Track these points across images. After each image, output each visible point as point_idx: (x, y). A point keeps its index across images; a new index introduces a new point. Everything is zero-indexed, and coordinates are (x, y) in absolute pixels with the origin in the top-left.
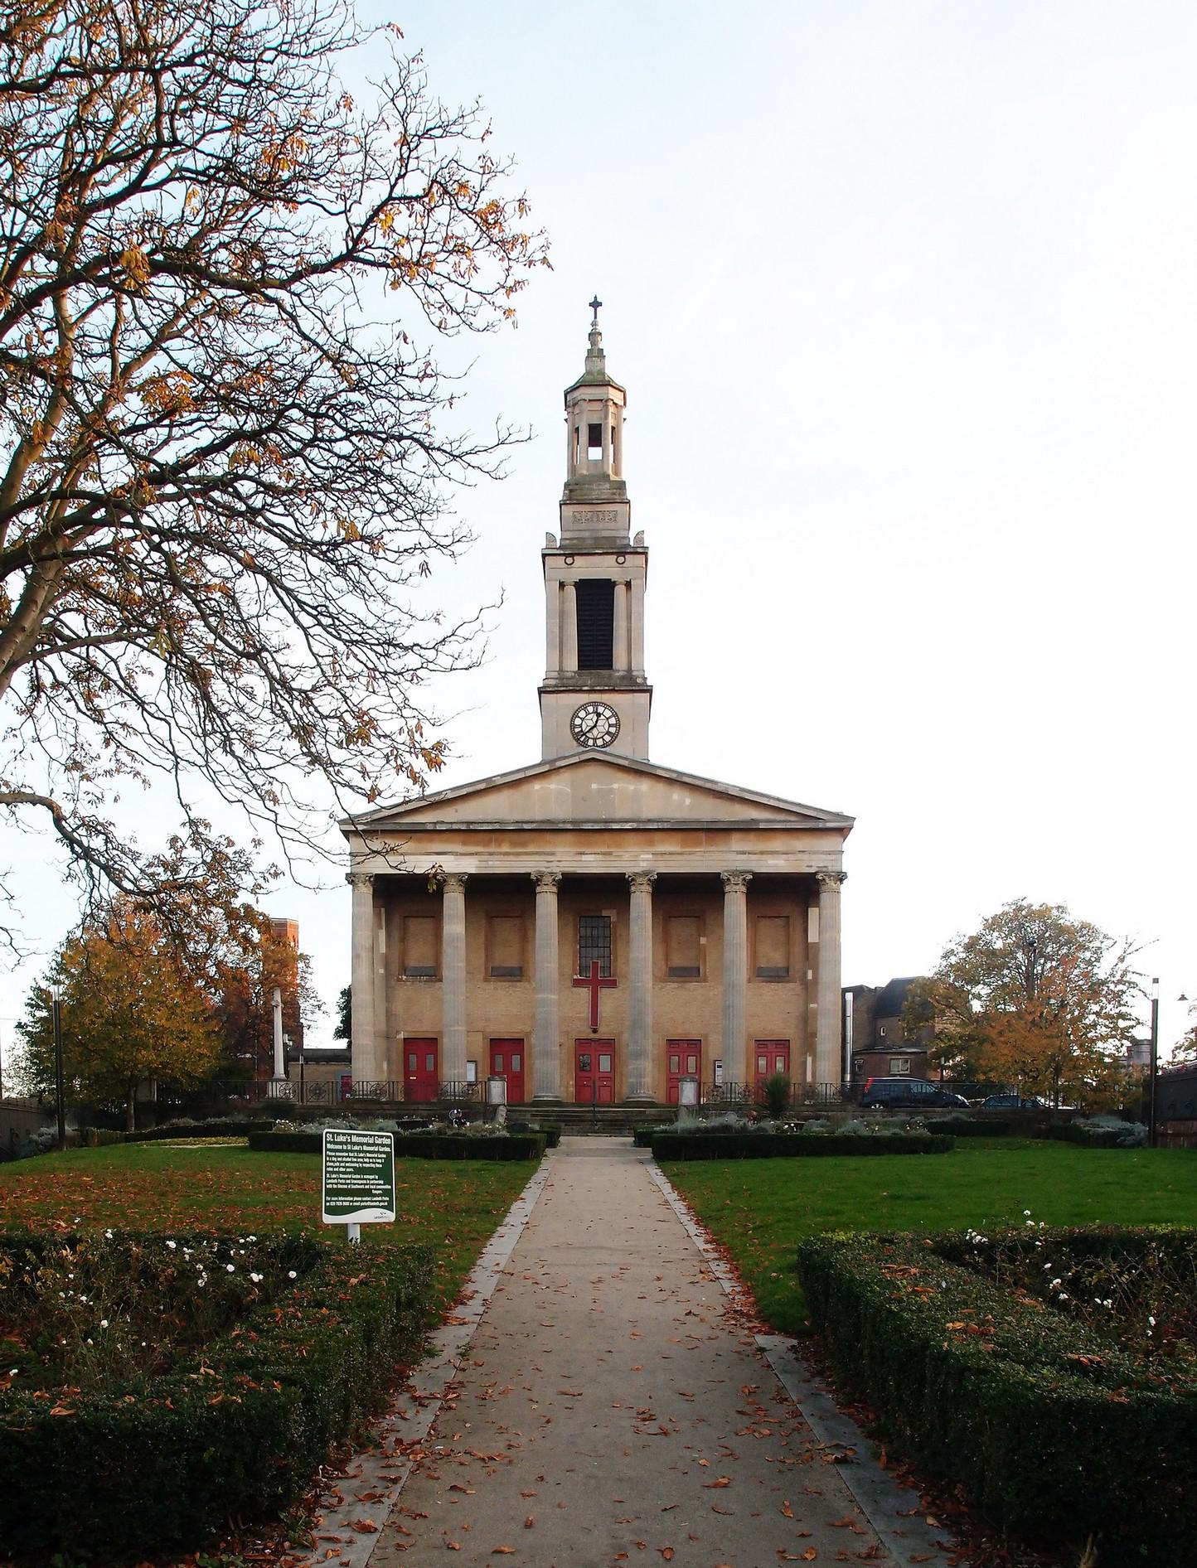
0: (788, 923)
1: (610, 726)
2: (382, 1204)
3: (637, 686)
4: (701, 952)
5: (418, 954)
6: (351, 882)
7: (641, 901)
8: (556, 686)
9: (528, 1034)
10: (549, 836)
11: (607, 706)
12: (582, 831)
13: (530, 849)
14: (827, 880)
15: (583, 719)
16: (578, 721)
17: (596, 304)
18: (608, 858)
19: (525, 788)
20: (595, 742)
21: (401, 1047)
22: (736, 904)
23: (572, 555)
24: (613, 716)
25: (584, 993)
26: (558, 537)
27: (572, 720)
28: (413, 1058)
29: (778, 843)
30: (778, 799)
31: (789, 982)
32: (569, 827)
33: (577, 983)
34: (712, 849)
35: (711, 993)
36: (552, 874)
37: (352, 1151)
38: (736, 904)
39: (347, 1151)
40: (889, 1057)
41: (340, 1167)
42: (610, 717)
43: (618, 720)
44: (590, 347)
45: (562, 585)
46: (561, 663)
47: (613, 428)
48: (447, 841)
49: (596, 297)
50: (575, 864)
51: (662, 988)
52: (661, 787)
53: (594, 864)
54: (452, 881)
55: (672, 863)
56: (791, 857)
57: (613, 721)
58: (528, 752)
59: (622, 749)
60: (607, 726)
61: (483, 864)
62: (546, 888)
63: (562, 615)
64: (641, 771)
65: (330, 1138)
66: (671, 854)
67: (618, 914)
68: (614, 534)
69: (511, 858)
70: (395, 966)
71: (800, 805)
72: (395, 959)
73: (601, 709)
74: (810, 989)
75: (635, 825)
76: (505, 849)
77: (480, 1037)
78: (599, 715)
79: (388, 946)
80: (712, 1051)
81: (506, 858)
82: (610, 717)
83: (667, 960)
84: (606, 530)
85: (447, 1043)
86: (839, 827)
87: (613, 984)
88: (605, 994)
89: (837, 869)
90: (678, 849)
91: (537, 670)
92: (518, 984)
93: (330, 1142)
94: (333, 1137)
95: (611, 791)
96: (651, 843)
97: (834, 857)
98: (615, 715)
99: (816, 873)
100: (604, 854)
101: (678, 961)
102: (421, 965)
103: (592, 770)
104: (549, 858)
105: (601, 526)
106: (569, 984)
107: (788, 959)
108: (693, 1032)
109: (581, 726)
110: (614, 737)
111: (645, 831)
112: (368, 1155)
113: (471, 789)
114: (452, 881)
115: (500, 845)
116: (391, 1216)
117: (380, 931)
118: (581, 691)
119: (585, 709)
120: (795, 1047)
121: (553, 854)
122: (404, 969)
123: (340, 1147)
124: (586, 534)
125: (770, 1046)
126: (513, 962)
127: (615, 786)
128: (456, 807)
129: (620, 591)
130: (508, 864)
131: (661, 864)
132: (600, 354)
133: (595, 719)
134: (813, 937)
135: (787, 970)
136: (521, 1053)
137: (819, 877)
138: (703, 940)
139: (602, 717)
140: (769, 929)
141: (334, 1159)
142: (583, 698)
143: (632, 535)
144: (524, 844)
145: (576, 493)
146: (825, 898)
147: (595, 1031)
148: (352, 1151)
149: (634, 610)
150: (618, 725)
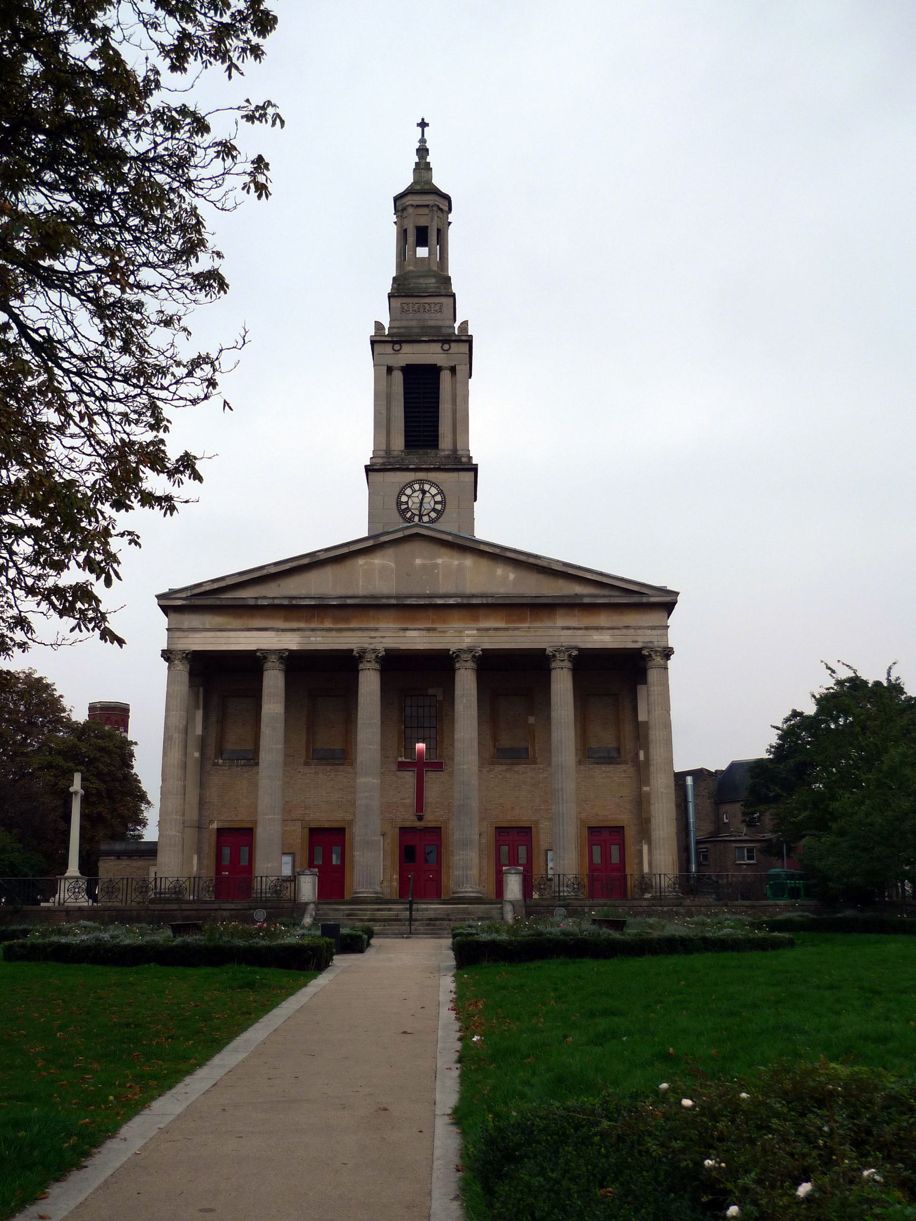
1: (436, 503)
5: (235, 738)
8: (383, 464)
11: (432, 484)
15: (409, 497)
17: (423, 125)
19: (349, 564)
23: (400, 342)
27: (399, 497)
28: (226, 851)
29: (603, 619)
36: (374, 651)
42: (436, 495)
43: (444, 497)
45: (390, 370)
52: (484, 564)
53: (418, 640)
54: (273, 658)
57: (438, 498)
59: (448, 526)
63: (389, 398)
68: (440, 323)
69: (334, 634)
70: (211, 751)
73: (427, 487)
78: (424, 492)
82: (436, 495)
85: (261, 835)
88: (430, 777)
89: (662, 644)
95: (436, 566)
96: (476, 619)
97: (659, 632)
98: (441, 492)
100: (428, 630)
103: (417, 547)
104: (373, 634)
105: (427, 316)
109: (407, 503)
110: (440, 513)
114: (273, 658)
118: (408, 470)
119: (411, 487)
124: (414, 323)
127: (439, 561)
129: (445, 376)
130: (330, 640)
131: (486, 639)
133: (421, 496)
139: (428, 495)
142: (410, 476)
144: (347, 620)
147: (420, 818)
150: (443, 502)
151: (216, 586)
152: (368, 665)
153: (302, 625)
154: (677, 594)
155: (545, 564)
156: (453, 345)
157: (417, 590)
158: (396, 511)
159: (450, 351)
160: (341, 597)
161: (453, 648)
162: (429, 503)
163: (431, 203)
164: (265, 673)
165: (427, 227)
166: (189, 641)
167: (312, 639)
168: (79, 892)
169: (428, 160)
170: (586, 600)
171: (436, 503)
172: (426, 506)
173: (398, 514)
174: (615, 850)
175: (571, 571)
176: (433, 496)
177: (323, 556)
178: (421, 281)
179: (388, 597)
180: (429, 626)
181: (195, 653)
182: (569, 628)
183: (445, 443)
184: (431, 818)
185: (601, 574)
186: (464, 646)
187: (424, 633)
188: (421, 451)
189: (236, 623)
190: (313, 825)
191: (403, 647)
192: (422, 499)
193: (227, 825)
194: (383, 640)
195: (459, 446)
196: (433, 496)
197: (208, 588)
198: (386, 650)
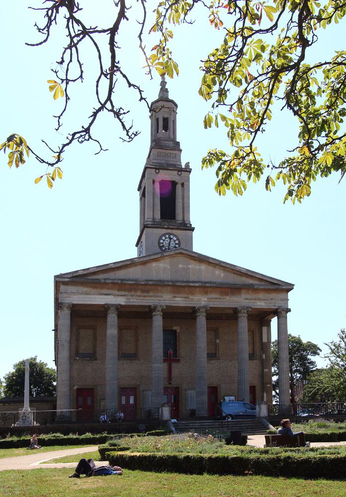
8: (152, 224)
9: (139, 386)
11: (175, 235)
12: (176, 287)
13: (151, 294)
15: (164, 240)
19: (148, 265)
23: (159, 169)
24: (177, 240)
27: (159, 240)
29: (261, 295)
31: (254, 360)
32: (170, 284)
34: (156, 294)
35: (221, 365)
43: (179, 242)
45: (154, 182)
46: (153, 216)
49: (36, 356)
50: (172, 302)
52: (211, 268)
53: (181, 302)
54: (113, 309)
55: (215, 303)
56: (267, 302)
57: (177, 242)
61: (127, 301)
66: (216, 298)
69: (142, 298)
73: (172, 237)
76: (139, 293)
81: (139, 298)
84: (172, 161)
87: (178, 361)
88: (174, 365)
89: (286, 307)
90: (218, 296)
92: (134, 361)
95: (188, 268)
96: (206, 293)
98: (178, 239)
102: (86, 352)
104: (160, 299)
105: (169, 159)
109: (163, 243)
111: (205, 287)
114: (113, 309)
121: (162, 297)
122: (77, 354)
124: (163, 162)
127: (190, 266)
128: (115, 273)
129: (179, 187)
130: (140, 301)
131: (211, 303)
132: (167, 91)
133: (169, 241)
138: (218, 341)
139: (172, 240)
142: (165, 231)
144: (148, 291)
145: (156, 143)
147: (170, 384)
149: (185, 194)
151: (85, 272)
152: (158, 313)
153: (126, 293)
154: (294, 285)
155: (238, 269)
156: (183, 172)
158: (158, 247)
159: (182, 175)
160: (146, 280)
161: (197, 306)
162: (172, 244)
163: (170, 106)
164: (109, 316)
165: (168, 118)
166: (71, 299)
167: (132, 300)
168: (23, 417)
169: (166, 87)
171: (176, 244)
172: (171, 245)
173: (158, 248)
174: (124, 402)
175: (249, 273)
176: (175, 241)
178: (166, 142)
179: (168, 281)
180: (186, 296)
181: (74, 305)
182: (247, 299)
183: (179, 217)
184: (174, 383)
185: (262, 275)
188: (169, 220)
189: (93, 291)
190: (122, 386)
191: (174, 305)
192: (170, 242)
193: (82, 387)
194: (165, 302)
196: (175, 241)
197: (81, 273)
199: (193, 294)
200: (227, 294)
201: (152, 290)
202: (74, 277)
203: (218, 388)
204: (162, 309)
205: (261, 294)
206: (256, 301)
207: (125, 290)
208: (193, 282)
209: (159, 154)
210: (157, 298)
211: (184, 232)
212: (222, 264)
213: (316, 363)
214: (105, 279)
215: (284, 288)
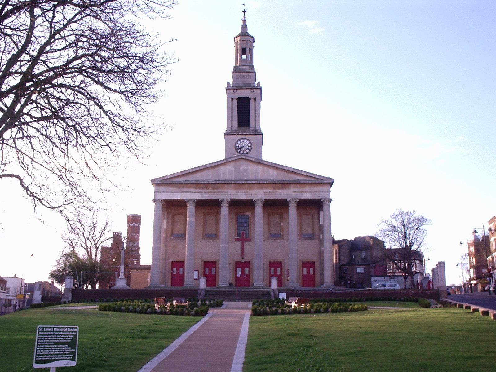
0: (313, 217)
1: (249, 146)
2: (68, 358)
3: (258, 133)
4: (281, 229)
6: (154, 202)
7: (259, 209)
8: (230, 133)
10: (226, 186)
11: (247, 140)
12: (238, 184)
14: (325, 201)
15: (239, 144)
16: (237, 145)
17: (244, 11)
18: (247, 194)
19: (217, 168)
20: (243, 152)
21: (170, 264)
22: (293, 211)
25: (239, 244)
26: (231, 83)
27: (235, 144)
29: (307, 188)
30: (307, 172)
31: (313, 239)
33: (236, 240)
37: (53, 335)
38: (293, 211)
39: (50, 335)
40: (356, 266)
41: (46, 342)
44: (242, 24)
45: (232, 99)
47: (250, 49)
48: (189, 187)
51: (268, 242)
56: (312, 193)
57: (250, 145)
58: (221, 156)
59: (252, 155)
60: (247, 147)
62: (224, 205)
64: (259, 162)
65: (41, 329)
66: (269, 192)
67: (251, 214)
68: (250, 82)
69: (212, 193)
70: (169, 234)
71: (314, 174)
72: (170, 230)
74: (321, 242)
75: (256, 182)
76: (210, 190)
77: (200, 261)
79: (167, 226)
80: (286, 266)
83: (269, 231)
84: (248, 81)
86: (330, 183)
87: (249, 240)
88: (246, 243)
89: (329, 197)
90: (272, 191)
91: (223, 127)
93: (41, 331)
94: (43, 329)
96: (262, 188)
97: (327, 193)
98: (250, 143)
99: (321, 199)
100: (246, 192)
101: (273, 231)
104: (226, 194)
105: (246, 79)
106: (234, 240)
107: (313, 230)
108: (279, 258)
110: (250, 150)
111: (260, 184)
112: (63, 336)
113: (198, 169)
115: (208, 189)
116: (74, 364)
117: (165, 220)
120: (317, 265)
121: (227, 192)
122: (172, 234)
123: (47, 333)
125: (308, 264)
126: (213, 232)
127: (249, 168)
129: (252, 101)
130: (216, 196)
134: (321, 223)
135: (313, 235)
136: (215, 267)
137: (322, 200)
138: (282, 224)
140: (307, 219)
141: (43, 339)
142: (240, 137)
143: (256, 83)
144: (216, 189)
145: (237, 70)
146: (325, 208)
147: (243, 258)
148: (53, 335)
150: (251, 146)
153: (201, 190)
156: (255, 90)
157: (242, 178)
170: (302, 182)
171: (249, 146)
173: (235, 150)
174: (311, 270)
177: (208, 166)
179: (232, 181)
186: (258, 198)
187: (244, 193)
189: (178, 189)
190: (205, 261)
193: (175, 260)
195: (257, 128)
198: (231, 199)
199: (251, 189)
200: (279, 188)
201: (220, 188)
202: (164, 180)
203: (283, 262)
204: (227, 202)
205: (307, 188)
206: (302, 193)
207: (199, 188)
208: (251, 181)
209: (238, 76)
210: (224, 193)
211: (255, 136)
212: (274, 165)
213: (50, 272)
214: (185, 181)
215: (334, 179)
